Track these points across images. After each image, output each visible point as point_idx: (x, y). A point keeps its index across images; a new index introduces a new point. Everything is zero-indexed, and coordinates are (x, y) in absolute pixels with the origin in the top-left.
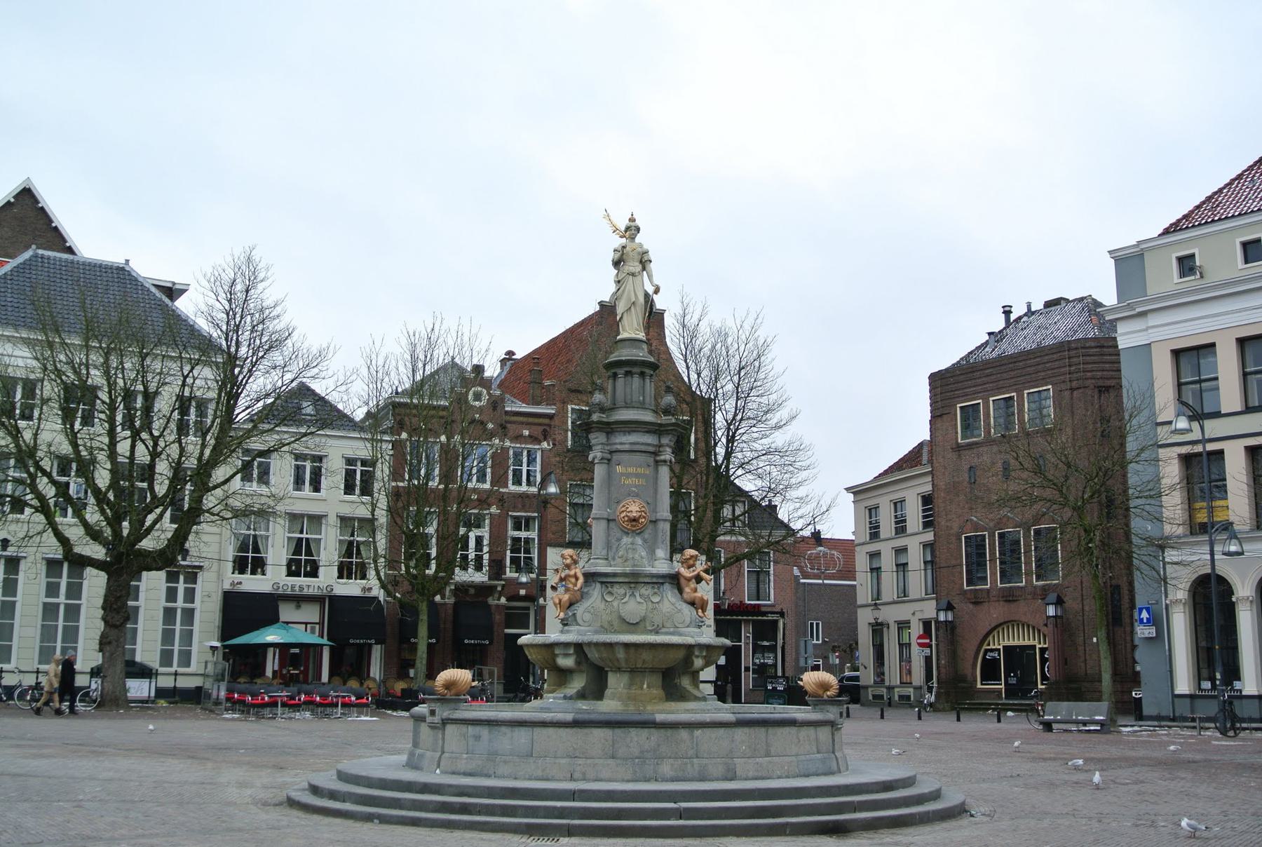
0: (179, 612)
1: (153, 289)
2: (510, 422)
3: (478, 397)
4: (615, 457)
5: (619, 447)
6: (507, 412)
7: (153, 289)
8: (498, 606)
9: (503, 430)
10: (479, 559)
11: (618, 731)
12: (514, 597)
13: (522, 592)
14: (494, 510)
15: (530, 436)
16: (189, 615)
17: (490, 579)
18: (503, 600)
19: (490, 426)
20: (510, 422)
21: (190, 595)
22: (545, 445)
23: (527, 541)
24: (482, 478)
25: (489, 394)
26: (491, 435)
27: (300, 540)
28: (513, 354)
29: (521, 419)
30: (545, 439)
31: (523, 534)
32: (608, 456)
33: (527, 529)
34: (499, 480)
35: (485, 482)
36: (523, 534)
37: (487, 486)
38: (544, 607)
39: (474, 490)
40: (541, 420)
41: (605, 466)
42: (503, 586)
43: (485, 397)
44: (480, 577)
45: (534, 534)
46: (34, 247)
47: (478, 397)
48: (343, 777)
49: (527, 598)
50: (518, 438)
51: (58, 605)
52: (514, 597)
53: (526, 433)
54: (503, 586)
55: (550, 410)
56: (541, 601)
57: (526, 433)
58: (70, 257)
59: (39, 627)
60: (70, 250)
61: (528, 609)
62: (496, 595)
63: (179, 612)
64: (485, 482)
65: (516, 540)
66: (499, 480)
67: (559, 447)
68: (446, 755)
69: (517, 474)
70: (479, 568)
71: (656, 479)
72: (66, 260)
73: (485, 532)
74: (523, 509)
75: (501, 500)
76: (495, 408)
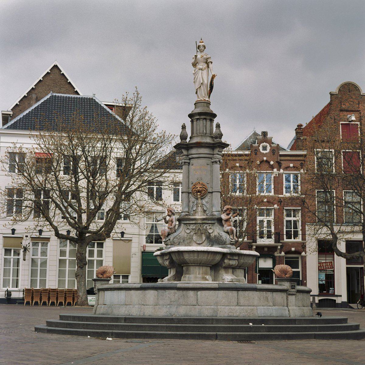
0: (67, 261)
1: (105, 107)
2: (282, 160)
3: (265, 148)
4: (192, 161)
5: (193, 156)
6: (281, 156)
7: (105, 107)
8: (280, 257)
9: (279, 165)
10: (269, 232)
11: (160, 292)
12: (288, 252)
13: (293, 249)
14: (276, 206)
15: (294, 167)
16: (44, 263)
17: (247, 240)
18: (283, 254)
19: (272, 163)
20: (282, 160)
21: (44, 253)
22: (302, 171)
23: (295, 222)
24: (269, 191)
25: (271, 146)
26: (272, 167)
27: (153, 224)
28: (302, 126)
29: (289, 158)
30: (302, 168)
31: (292, 219)
32: (188, 161)
33: (268, 215)
34: (278, 190)
35: (270, 192)
36: (292, 219)
37: (272, 194)
38: (305, 257)
39: (265, 197)
40: (299, 158)
41: (187, 166)
42: (281, 246)
43: (269, 148)
44: (271, 242)
45: (299, 217)
46: (51, 92)
47: (265, 148)
48: (62, 317)
49: (296, 252)
50: (287, 168)
51: (66, 260)
52: (288, 252)
53: (291, 165)
54: (281, 246)
55: (304, 153)
56: (303, 254)
57: (291, 165)
58: (76, 96)
59: (58, 271)
60: (77, 93)
61: (298, 258)
62: (278, 251)
63: (67, 261)
64: (270, 192)
65: (289, 222)
66: (278, 190)
67: (310, 172)
68: (99, 306)
69: (288, 188)
70: (269, 237)
71: (212, 171)
72: (74, 98)
73: (271, 218)
74: (292, 205)
75: (280, 202)
76: (274, 154)
